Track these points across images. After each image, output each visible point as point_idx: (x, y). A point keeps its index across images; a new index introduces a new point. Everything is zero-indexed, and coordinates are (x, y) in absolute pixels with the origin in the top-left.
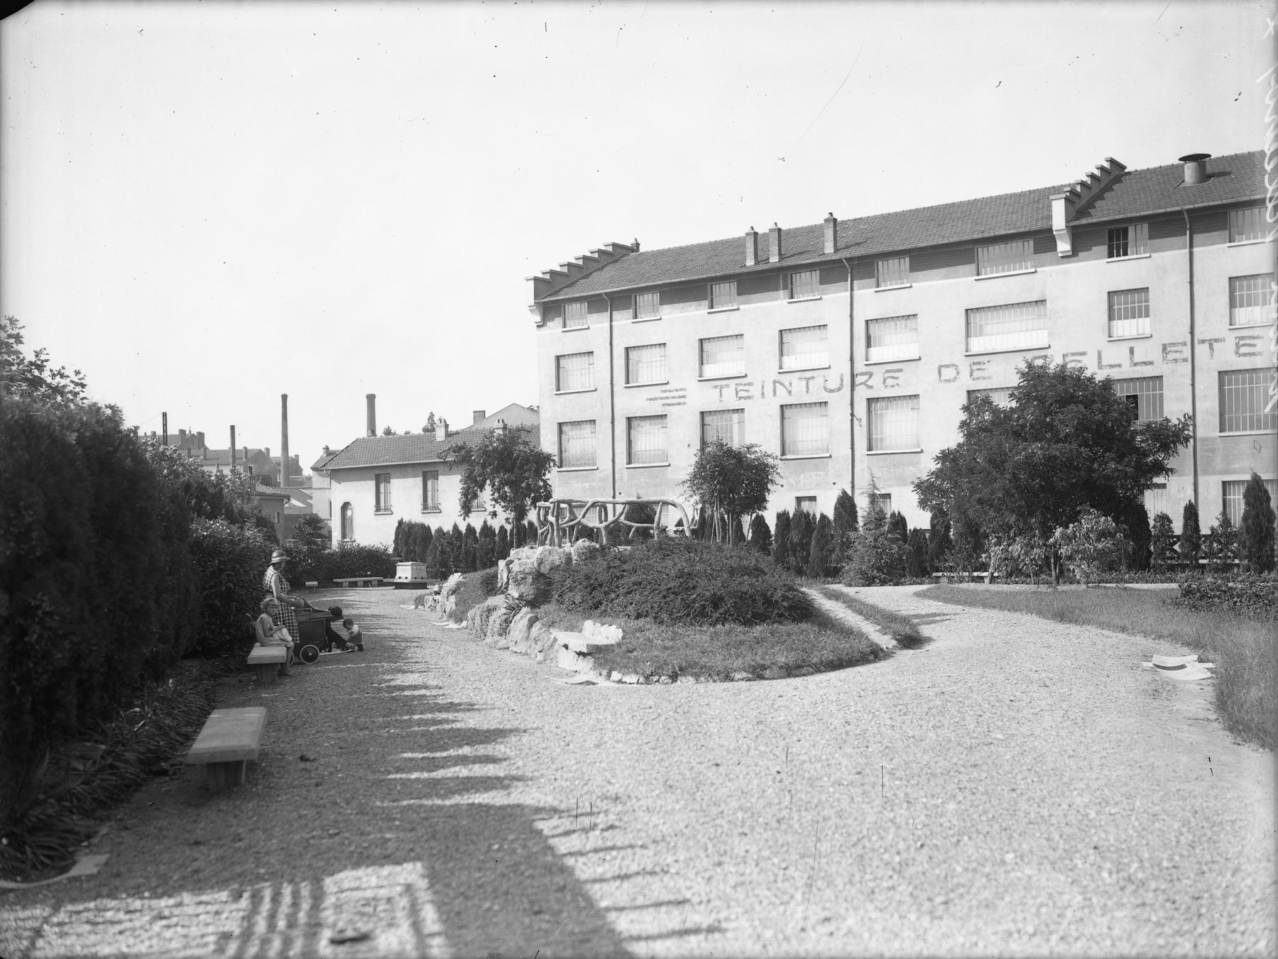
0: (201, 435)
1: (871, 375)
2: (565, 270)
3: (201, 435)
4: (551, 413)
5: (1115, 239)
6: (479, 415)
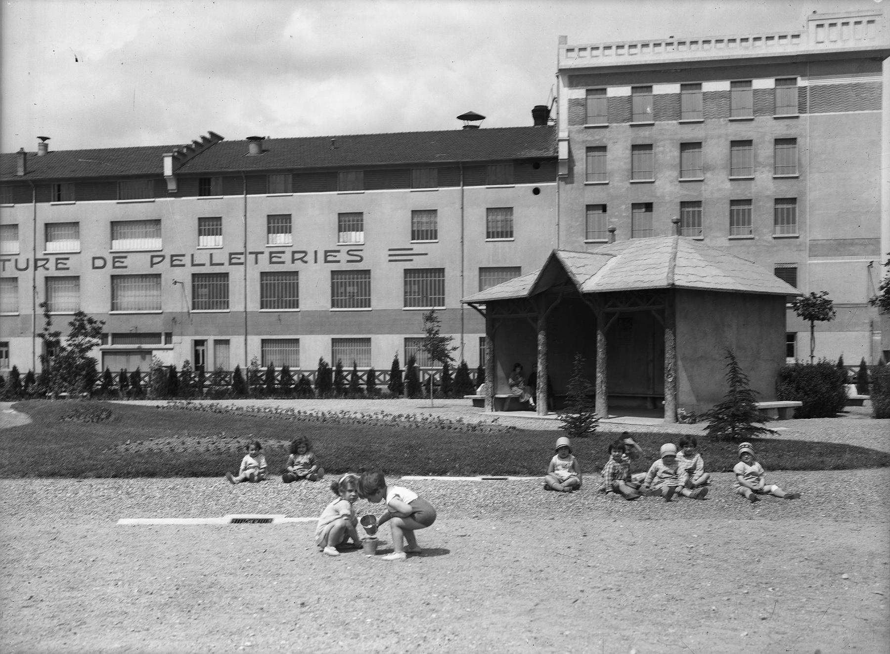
1: (47, 260)
5: (201, 185)
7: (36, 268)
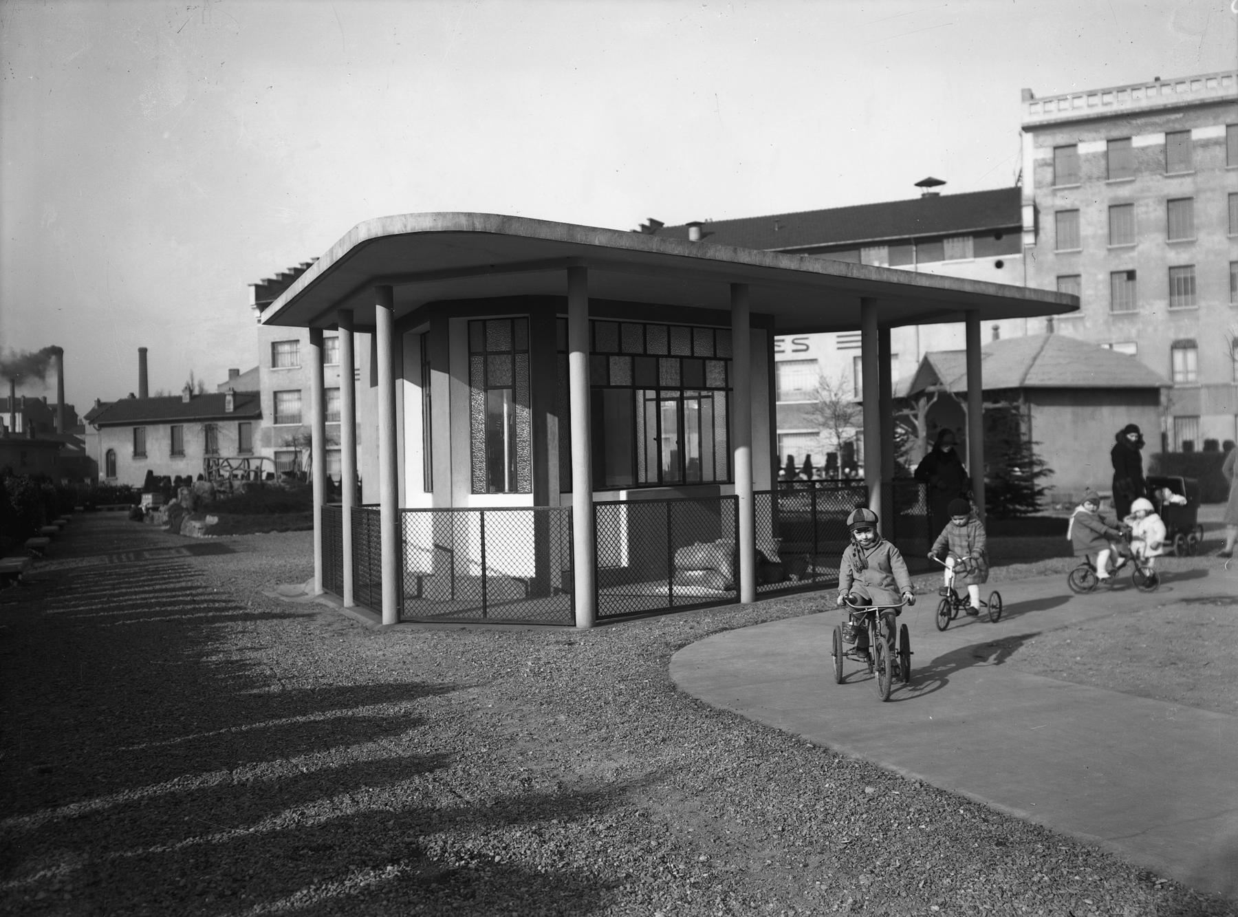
4: (267, 383)
6: (234, 373)
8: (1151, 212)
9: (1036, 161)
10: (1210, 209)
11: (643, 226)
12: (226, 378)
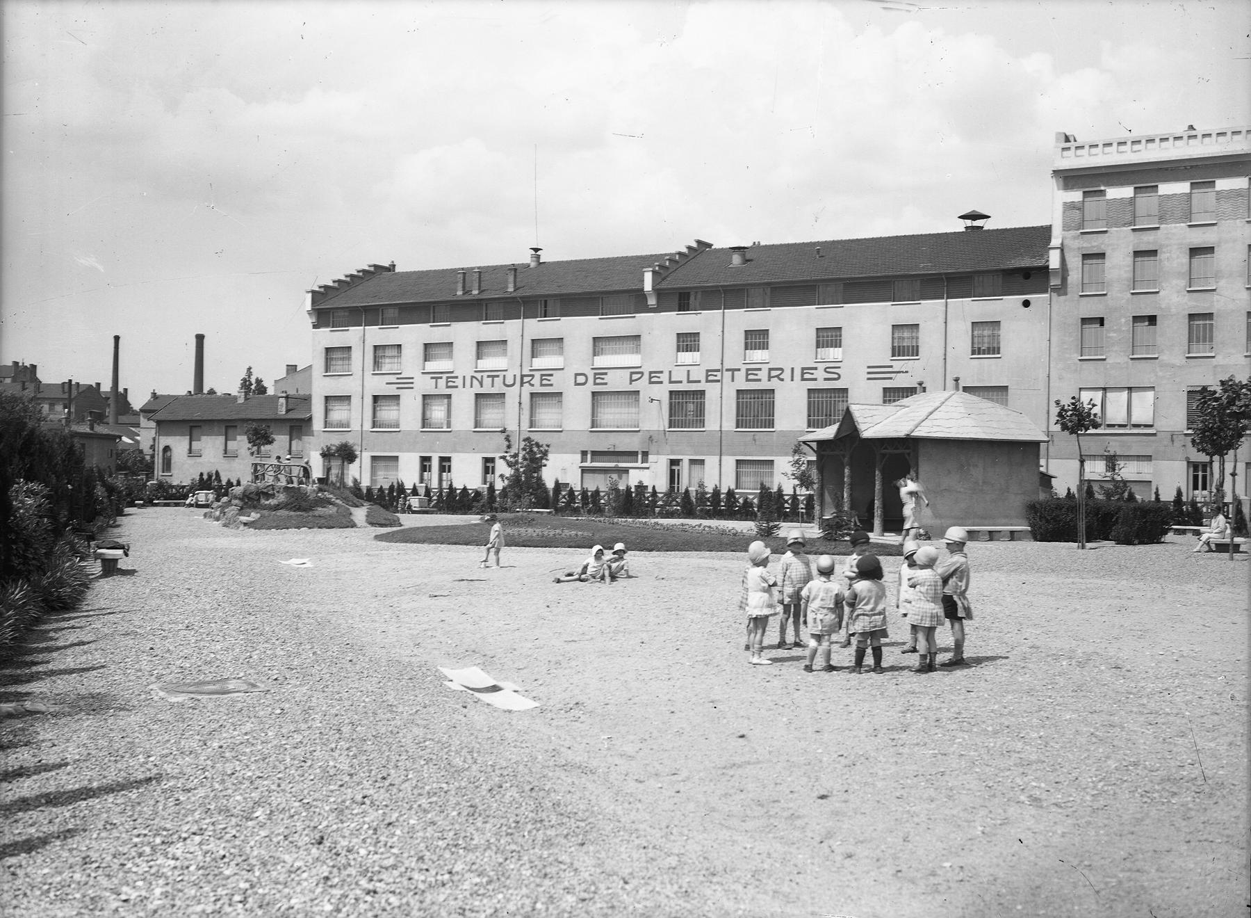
0: (34, 367)
2: (336, 285)
3: (34, 367)
5: (681, 300)
6: (292, 369)
7: (522, 384)
8: (1174, 259)
9: (1065, 204)
10: (1230, 257)
11: (689, 248)
12: (282, 373)
